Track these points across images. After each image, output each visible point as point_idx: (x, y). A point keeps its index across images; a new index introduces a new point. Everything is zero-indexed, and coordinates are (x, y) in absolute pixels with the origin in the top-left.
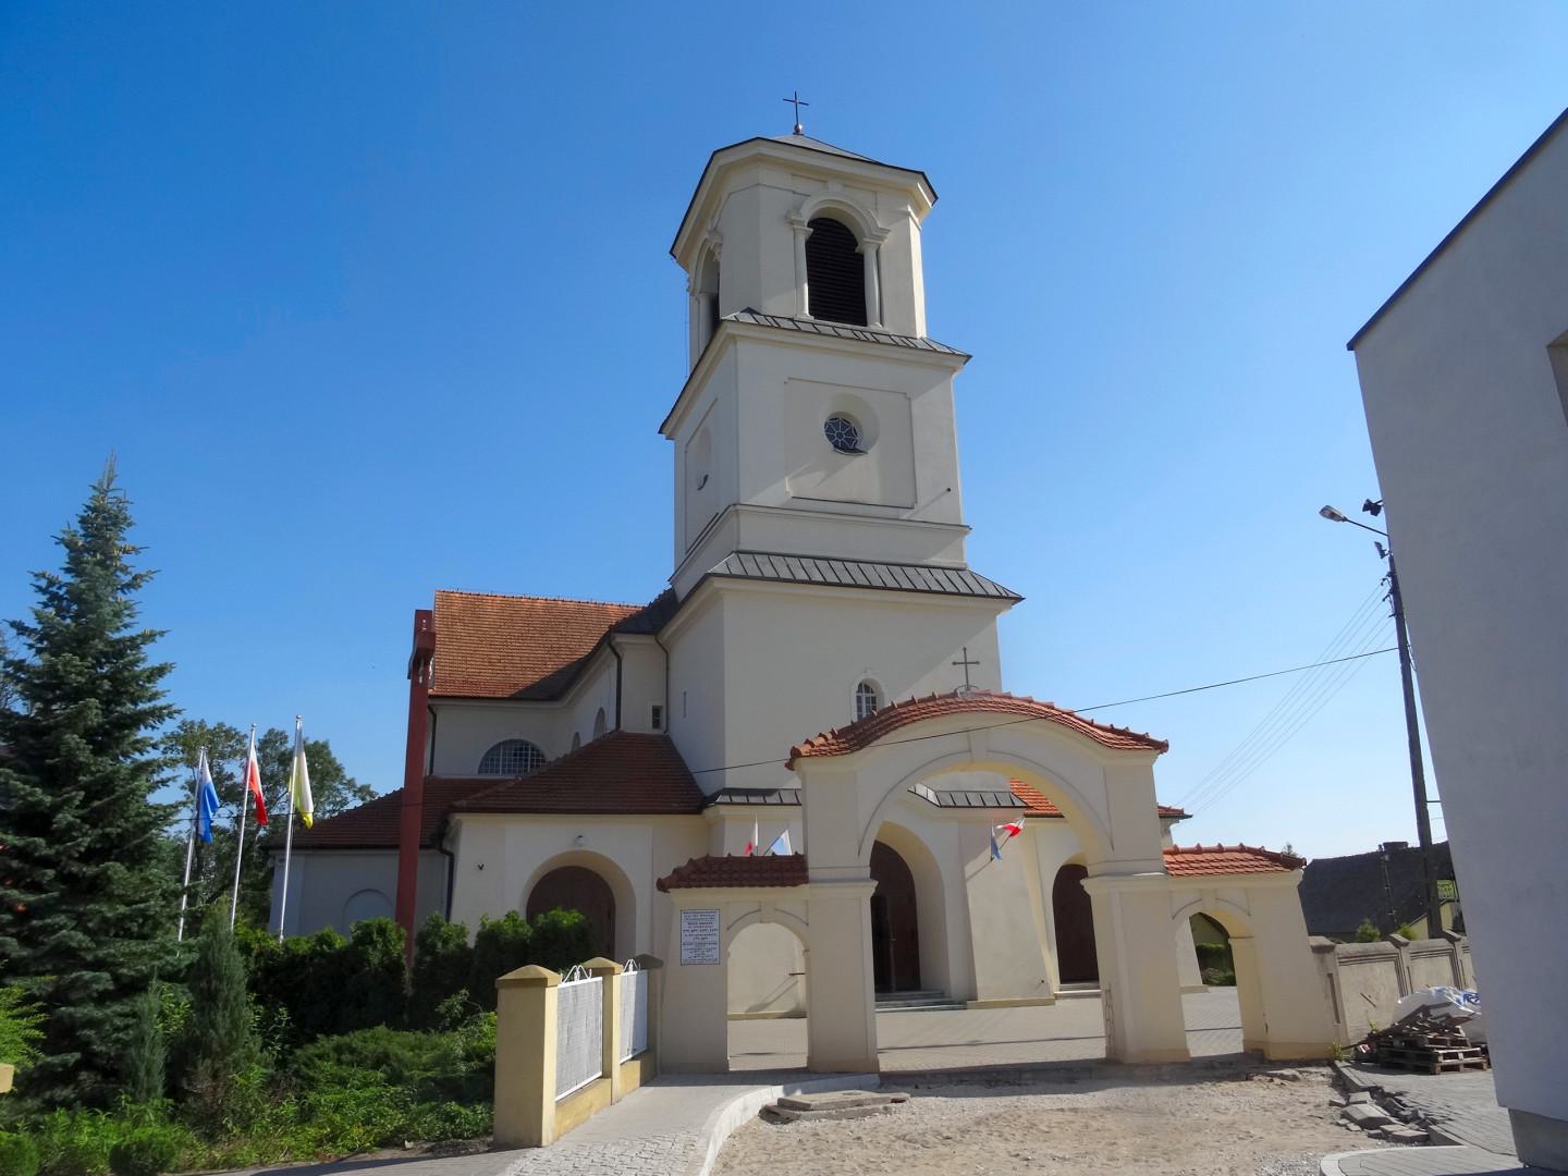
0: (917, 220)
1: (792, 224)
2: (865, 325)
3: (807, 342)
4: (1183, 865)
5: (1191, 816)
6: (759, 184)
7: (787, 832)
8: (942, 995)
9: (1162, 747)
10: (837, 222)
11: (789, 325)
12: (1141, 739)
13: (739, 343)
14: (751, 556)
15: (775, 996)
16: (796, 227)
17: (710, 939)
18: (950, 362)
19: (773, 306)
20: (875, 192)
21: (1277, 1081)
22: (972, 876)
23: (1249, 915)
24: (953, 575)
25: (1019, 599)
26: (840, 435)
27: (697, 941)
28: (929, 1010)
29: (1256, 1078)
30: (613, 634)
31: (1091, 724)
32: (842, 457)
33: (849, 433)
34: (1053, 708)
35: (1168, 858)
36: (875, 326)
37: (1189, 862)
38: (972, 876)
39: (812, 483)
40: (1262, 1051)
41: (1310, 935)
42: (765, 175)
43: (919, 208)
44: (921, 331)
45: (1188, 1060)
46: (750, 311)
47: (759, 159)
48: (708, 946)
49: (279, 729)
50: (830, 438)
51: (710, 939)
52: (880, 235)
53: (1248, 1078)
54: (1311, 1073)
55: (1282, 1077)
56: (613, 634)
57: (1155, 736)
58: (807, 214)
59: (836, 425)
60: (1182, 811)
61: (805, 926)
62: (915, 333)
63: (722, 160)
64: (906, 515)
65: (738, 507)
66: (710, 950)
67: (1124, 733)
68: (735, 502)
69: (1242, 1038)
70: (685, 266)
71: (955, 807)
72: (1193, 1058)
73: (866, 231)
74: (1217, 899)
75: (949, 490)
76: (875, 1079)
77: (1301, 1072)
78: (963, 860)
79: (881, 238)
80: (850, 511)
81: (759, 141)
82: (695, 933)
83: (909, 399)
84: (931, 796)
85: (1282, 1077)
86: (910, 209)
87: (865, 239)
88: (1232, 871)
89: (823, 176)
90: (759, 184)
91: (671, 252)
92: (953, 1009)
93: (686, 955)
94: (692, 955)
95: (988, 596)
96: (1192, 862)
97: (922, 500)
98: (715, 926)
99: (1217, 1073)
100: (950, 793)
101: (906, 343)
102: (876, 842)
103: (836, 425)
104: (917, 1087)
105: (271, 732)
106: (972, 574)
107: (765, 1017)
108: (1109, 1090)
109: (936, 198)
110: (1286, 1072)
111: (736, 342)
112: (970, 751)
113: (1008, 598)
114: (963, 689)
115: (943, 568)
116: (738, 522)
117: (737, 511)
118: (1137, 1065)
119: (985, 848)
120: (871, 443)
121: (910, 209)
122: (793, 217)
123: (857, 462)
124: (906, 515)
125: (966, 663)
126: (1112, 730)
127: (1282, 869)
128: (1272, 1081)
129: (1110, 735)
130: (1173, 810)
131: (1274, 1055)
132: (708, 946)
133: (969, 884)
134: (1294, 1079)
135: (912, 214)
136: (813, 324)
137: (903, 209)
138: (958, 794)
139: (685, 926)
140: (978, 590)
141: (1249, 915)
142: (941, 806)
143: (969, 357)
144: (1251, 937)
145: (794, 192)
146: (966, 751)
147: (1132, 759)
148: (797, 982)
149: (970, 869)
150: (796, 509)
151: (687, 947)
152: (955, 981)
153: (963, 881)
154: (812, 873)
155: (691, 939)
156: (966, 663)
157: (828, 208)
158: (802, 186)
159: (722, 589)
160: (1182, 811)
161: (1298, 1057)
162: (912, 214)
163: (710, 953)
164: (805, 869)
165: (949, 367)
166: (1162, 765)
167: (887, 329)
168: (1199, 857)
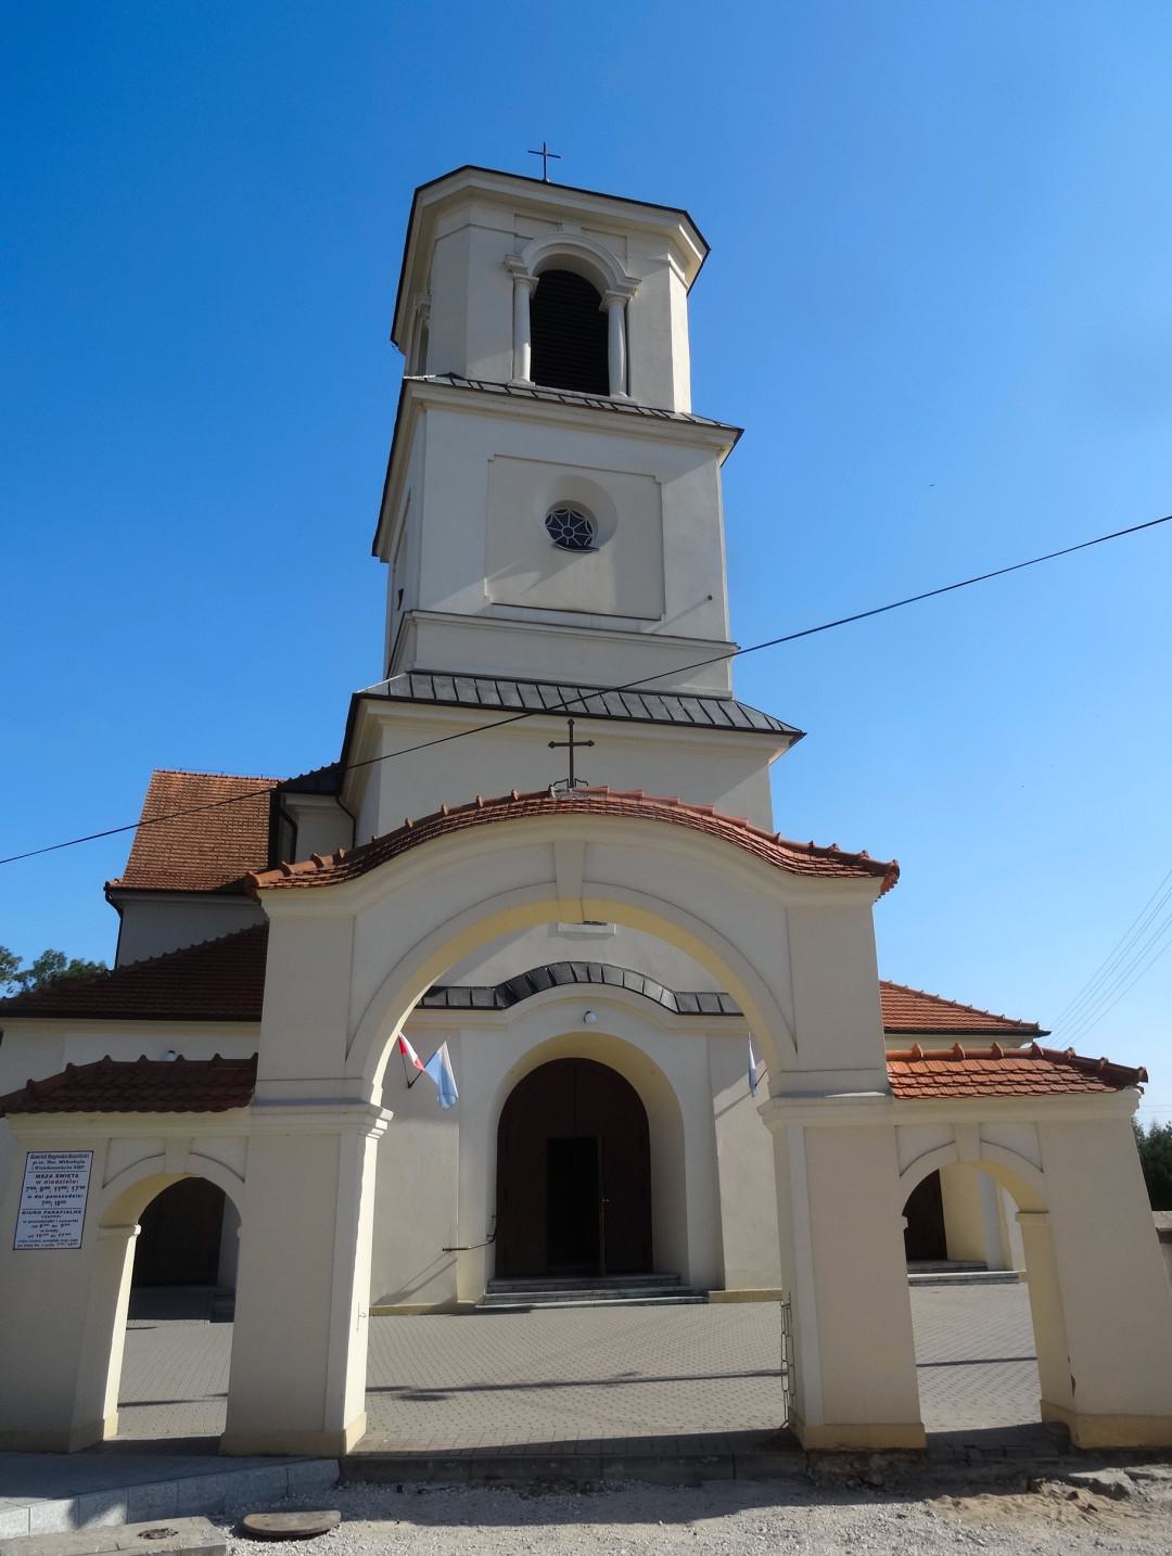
0: (682, 275)
1: (511, 271)
2: (608, 395)
3: (521, 410)
4: (922, 1080)
5: (1048, 1033)
6: (470, 225)
7: (445, 1045)
8: (678, 1280)
9: (887, 874)
10: (577, 276)
11: (502, 389)
12: (859, 865)
13: (429, 412)
14: (450, 680)
15: (422, 1279)
16: (515, 275)
17: (71, 1203)
18: (715, 437)
19: (482, 369)
20: (625, 238)
21: (1085, 1496)
22: (721, 1113)
23: (104, 1186)
24: (711, 706)
25: (798, 735)
26: (568, 532)
27: (47, 1206)
28: (651, 1303)
29: (1045, 1488)
30: (283, 795)
31: (775, 840)
32: (564, 555)
33: (582, 529)
34: (710, 814)
35: (899, 1067)
36: (618, 395)
37: (933, 1074)
38: (721, 1113)
39: (523, 588)
40: (1066, 1428)
41: (1153, 1210)
42: (478, 214)
43: (684, 263)
44: (682, 404)
45: (921, 1444)
46: (452, 376)
47: (471, 194)
48: (65, 1217)
49: (57, 949)
50: (554, 534)
51: (71, 1203)
52: (628, 287)
53: (1032, 1489)
54: (1154, 1479)
55: (1097, 1488)
56: (283, 795)
57: (879, 856)
58: (532, 259)
59: (564, 519)
60: (1036, 1026)
61: (240, 1181)
62: (672, 402)
63: (428, 199)
64: (650, 628)
65: (415, 614)
66: (65, 1223)
67: (831, 853)
68: (414, 608)
69: (1039, 1397)
70: (404, 353)
71: (701, 1013)
72: (932, 1437)
73: (610, 282)
74: (982, 1141)
75: (710, 598)
76: (331, 1469)
77: (1134, 1477)
78: (711, 1092)
79: (630, 290)
80: (575, 623)
81: (468, 171)
82: (46, 1192)
83: (660, 484)
84: (667, 999)
85: (1097, 1488)
86: (670, 258)
87: (608, 292)
88: (1008, 1089)
89: (555, 217)
90: (470, 225)
91: (392, 339)
92: (687, 1302)
93: (25, 1231)
94: (38, 1231)
95: (754, 730)
96: (940, 1074)
97: (674, 606)
98: (83, 1180)
99: (973, 1474)
100: (696, 996)
101: (663, 416)
102: (258, 1018)
103: (564, 519)
104: (399, 1490)
105: (47, 953)
106: (739, 706)
107: (402, 1312)
108: (745, 1516)
109: (708, 249)
110: (1107, 1476)
111: (425, 411)
112: (555, 881)
113: (782, 733)
114: (564, 786)
115: (699, 698)
116: (416, 634)
117: (414, 619)
118: (824, 1453)
119: (743, 1074)
120: (606, 539)
121: (670, 258)
122: (512, 263)
123: (584, 561)
124: (650, 628)
125: (571, 744)
126: (811, 850)
127: (1101, 1086)
128: (1074, 1496)
129: (806, 857)
130: (1024, 1025)
131: (1087, 1437)
132: (65, 1217)
133: (718, 1123)
134: (1118, 1493)
135: (673, 263)
136: (532, 391)
137: (662, 257)
138: (708, 997)
139: (31, 1180)
140: (740, 721)
141: (104, 1186)
142: (680, 1013)
143: (740, 431)
144: (1046, 1212)
145: (516, 235)
146: (550, 882)
147: (838, 893)
148: (455, 1261)
149: (721, 1101)
150: (489, 620)
151: (28, 1217)
152: (695, 1263)
153: (711, 1117)
154: (261, 1089)
155: (36, 1204)
156: (571, 744)
157: (570, 256)
158: (525, 228)
159: (384, 717)
160: (1036, 1026)
161: (1133, 1442)
162: (673, 263)
163: (66, 1229)
164: (252, 1081)
165: (714, 445)
166: (888, 912)
167: (634, 399)
168: (954, 1066)
